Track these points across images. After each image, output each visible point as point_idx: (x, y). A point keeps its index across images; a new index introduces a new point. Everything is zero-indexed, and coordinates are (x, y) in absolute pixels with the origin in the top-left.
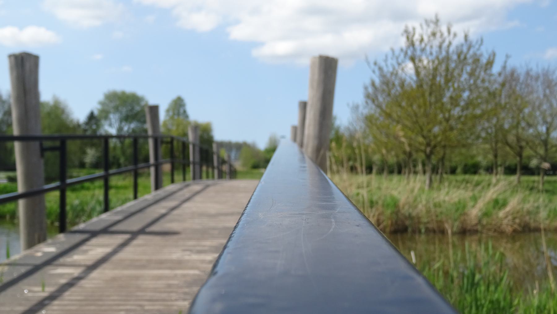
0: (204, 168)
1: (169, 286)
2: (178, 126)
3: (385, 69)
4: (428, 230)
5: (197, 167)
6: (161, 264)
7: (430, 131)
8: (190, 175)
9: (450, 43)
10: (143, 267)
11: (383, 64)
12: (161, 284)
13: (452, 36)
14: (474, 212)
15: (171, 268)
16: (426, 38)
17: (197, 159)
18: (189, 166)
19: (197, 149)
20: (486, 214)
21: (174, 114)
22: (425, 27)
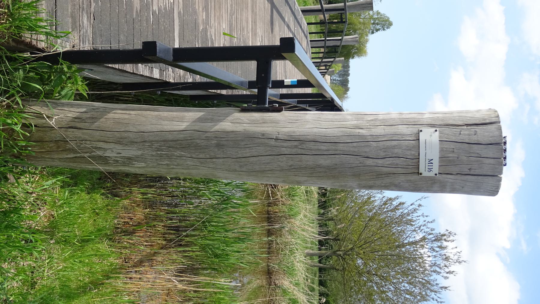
0: (322, 50)
1: (243, 29)
2: (364, 24)
3: (415, 215)
4: (270, 243)
5: (322, 44)
6: (254, 22)
7: (358, 254)
8: (315, 37)
9: (439, 273)
10: (253, 11)
11: (419, 213)
12: (244, 24)
13: (445, 275)
14: (286, 283)
15: (252, 29)
16: (443, 252)
17: (329, 44)
18: (54, 178)
19: (338, 43)
20: (285, 291)
21: (375, 19)
22: (455, 251)
